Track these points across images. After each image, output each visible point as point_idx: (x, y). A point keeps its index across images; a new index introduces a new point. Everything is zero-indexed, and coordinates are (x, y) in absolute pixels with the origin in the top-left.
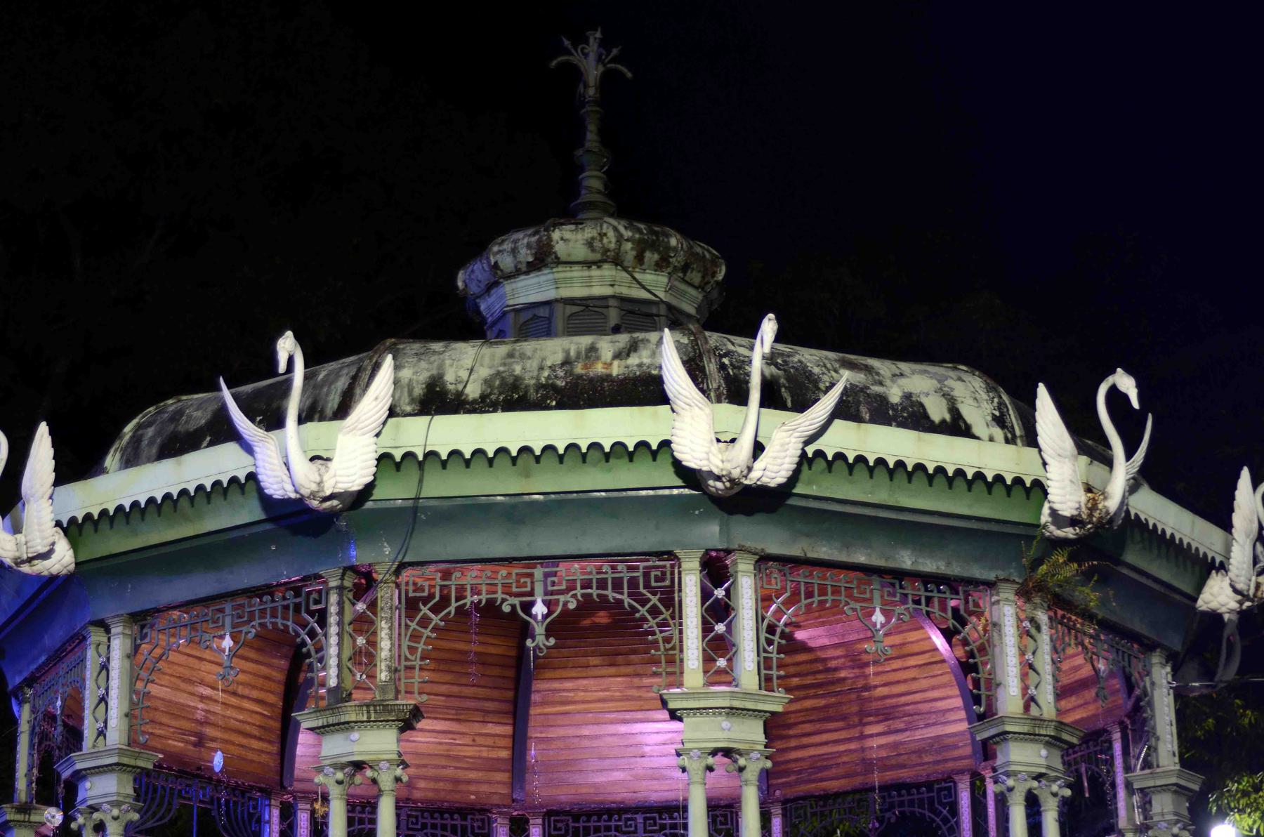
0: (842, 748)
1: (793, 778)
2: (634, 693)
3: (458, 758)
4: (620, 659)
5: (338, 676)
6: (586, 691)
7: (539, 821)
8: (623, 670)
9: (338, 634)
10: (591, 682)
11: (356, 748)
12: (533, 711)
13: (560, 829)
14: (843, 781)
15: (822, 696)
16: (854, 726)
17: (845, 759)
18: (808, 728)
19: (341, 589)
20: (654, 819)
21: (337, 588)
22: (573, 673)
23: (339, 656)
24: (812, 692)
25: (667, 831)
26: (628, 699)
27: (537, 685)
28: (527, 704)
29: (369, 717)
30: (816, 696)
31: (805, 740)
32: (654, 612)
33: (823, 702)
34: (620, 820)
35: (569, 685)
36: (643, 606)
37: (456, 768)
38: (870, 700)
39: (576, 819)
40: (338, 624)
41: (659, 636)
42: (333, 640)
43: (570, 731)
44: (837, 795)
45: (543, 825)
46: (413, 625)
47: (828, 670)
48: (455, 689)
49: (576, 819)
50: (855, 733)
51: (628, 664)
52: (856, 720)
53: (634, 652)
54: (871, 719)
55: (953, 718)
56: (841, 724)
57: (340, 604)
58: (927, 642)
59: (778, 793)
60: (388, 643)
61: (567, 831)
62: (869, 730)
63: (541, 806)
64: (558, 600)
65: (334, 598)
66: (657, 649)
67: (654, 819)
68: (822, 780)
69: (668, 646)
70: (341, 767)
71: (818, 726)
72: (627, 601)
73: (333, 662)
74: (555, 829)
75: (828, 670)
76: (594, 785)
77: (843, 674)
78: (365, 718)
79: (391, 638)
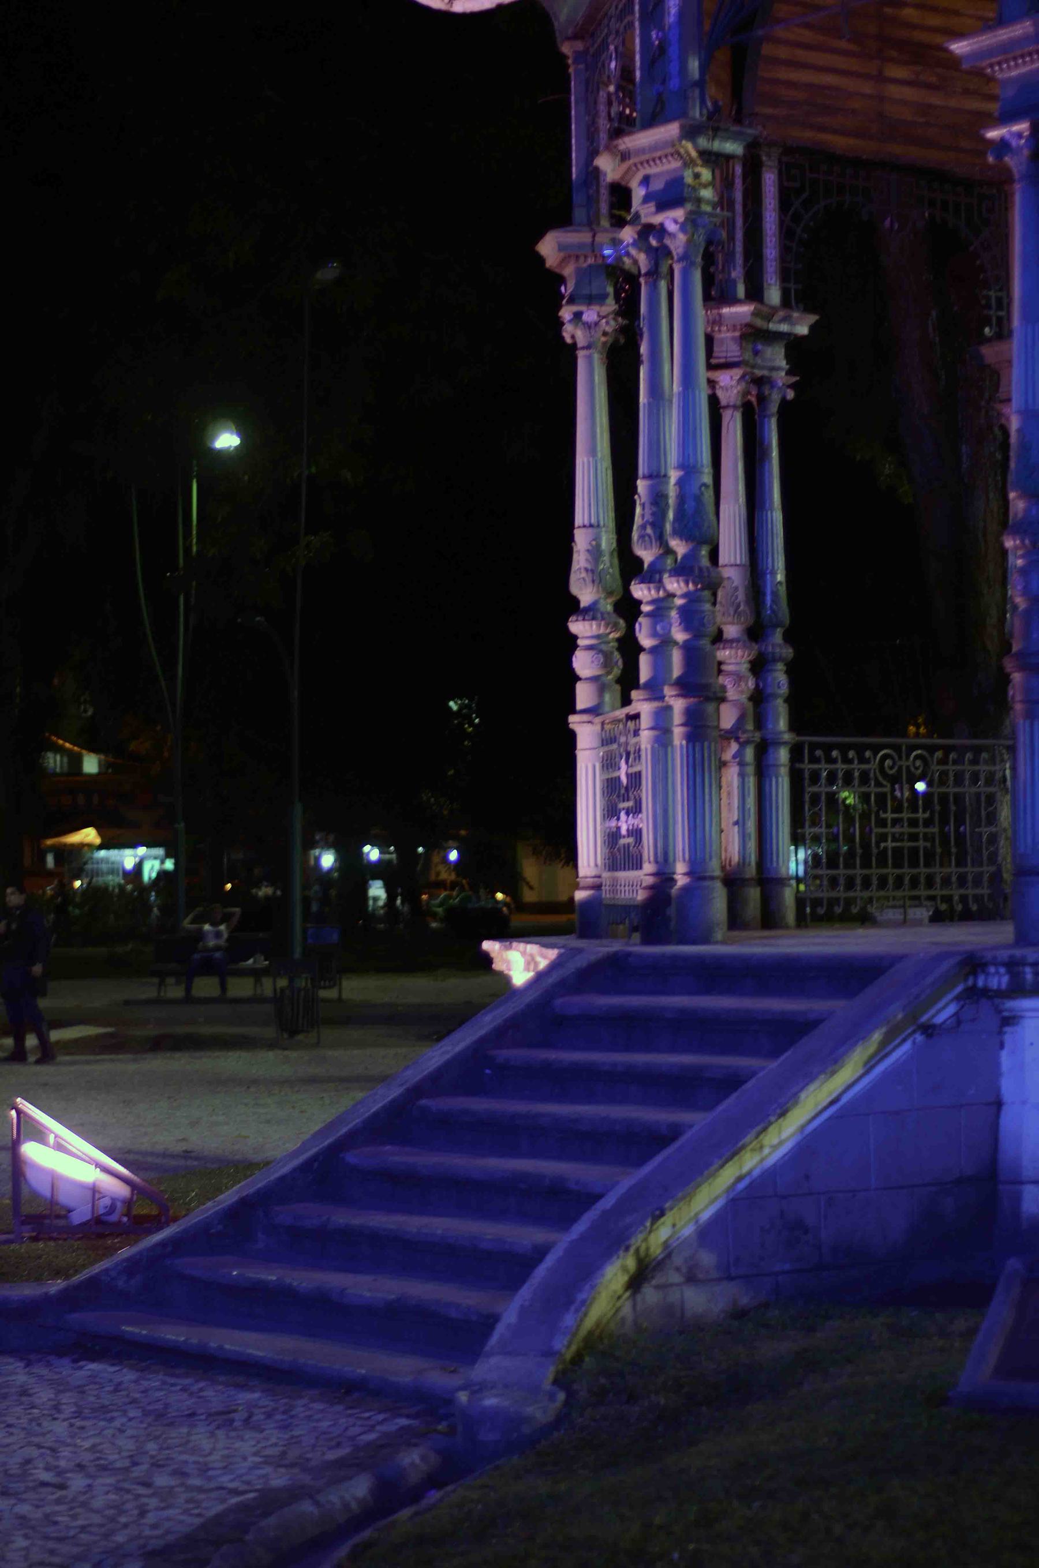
14: (852, 141)
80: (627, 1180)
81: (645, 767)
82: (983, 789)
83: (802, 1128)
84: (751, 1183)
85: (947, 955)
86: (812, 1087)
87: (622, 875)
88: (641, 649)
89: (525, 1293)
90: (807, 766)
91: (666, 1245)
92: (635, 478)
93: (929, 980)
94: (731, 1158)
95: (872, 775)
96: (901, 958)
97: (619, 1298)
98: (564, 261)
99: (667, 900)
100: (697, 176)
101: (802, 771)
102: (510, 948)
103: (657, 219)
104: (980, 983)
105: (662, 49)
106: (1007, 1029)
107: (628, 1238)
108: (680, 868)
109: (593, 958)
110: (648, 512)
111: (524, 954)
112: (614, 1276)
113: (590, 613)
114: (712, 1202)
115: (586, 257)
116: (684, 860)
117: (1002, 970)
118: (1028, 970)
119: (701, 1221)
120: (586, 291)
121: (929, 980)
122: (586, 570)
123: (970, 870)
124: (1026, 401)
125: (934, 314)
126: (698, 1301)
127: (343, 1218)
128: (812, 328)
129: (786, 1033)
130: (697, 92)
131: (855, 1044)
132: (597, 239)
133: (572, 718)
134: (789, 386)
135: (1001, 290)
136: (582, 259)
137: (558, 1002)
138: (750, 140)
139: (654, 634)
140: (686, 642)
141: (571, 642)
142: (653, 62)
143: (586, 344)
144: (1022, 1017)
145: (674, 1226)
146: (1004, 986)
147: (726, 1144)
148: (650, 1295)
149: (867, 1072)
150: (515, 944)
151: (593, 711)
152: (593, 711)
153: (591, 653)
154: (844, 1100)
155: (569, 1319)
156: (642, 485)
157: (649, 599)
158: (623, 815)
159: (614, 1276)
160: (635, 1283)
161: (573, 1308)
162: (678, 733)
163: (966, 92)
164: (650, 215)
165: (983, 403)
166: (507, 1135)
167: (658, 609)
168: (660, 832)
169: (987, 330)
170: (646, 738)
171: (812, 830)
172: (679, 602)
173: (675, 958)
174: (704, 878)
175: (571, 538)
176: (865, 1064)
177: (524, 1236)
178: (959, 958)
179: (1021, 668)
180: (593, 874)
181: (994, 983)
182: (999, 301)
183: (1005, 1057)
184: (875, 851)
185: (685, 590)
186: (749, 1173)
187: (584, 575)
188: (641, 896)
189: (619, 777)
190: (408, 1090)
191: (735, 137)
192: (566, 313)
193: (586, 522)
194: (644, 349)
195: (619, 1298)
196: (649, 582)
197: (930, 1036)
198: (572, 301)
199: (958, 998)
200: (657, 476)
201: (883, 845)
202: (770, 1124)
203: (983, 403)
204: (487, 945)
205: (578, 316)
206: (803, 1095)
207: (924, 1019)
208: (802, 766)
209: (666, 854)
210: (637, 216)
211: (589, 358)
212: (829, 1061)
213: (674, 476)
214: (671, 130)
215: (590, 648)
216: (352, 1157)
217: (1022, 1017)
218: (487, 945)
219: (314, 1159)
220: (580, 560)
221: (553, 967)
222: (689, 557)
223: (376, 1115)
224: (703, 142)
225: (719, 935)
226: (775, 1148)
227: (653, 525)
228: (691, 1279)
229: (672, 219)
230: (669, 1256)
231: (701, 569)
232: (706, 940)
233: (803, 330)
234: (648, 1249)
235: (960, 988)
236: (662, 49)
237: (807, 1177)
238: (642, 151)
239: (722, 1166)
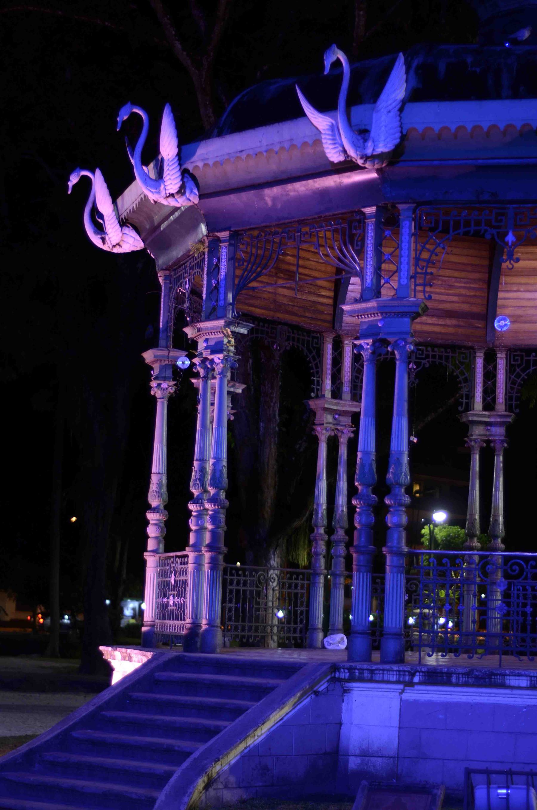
14: (263, 311)
32: (314, 358)
36: (521, 375)
38: (283, 261)
46: (513, 377)
55: (323, 293)
58: (512, 320)
64: (421, 362)
72: (305, 350)
74: (514, 360)
80: (202, 747)
81: (190, 579)
82: (299, 591)
83: (269, 730)
84: (249, 751)
85: (323, 664)
86: (274, 713)
87: (168, 622)
88: (191, 530)
89: (167, 788)
90: (228, 577)
91: (218, 773)
92: (193, 460)
93: (318, 673)
94: (243, 741)
95: (255, 582)
96: (305, 664)
97: (201, 792)
98: (154, 362)
99: (197, 634)
100: (229, 342)
101: (227, 579)
102: (116, 650)
103: (211, 357)
104: (337, 676)
105: (217, 288)
106: (345, 694)
107: (206, 769)
108: (204, 622)
109: (170, 657)
110: (198, 474)
111: (121, 653)
112: (201, 783)
113: (155, 510)
114: (235, 757)
115: (165, 361)
116: (206, 618)
117: (346, 671)
118: (357, 671)
119: (231, 764)
120: (163, 375)
121: (318, 673)
122: (156, 492)
123: (247, 624)
124: (364, 448)
125: (251, 361)
126: (228, 796)
127: (75, 758)
128: (243, 390)
129: (258, 693)
130: (231, 307)
131: (290, 697)
132: (170, 354)
133: (145, 554)
134: (232, 414)
135: (319, 377)
136: (163, 362)
137: (157, 674)
138: (250, 328)
139: (197, 525)
140: (212, 529)
141: (147, 523)
142: (211, 292)
143: (162, 397)
144: (352, 690)
145: (221, 765)
146: (346, 677)
147: (242, 734)
148: (212, 792)
149: (294, 709)
150: (118, 649)
151: (155, 551)
152: (155, 551)
153: (156, 527)
154: (285, 719)
155: (186, 799)
156: (195, 463)
157: (196, 510)
158: (171, 597)
159: (201, 783)
160: (207, 787)
161: (187, 795)
162: (206, 568)
163: (310, 293)
164: (206, 354)
165: (272, 404)
166: (140, 727)
167: (199, 514)
168: (195, 606)
169: (312, 394)
170: (190, 567)
171: (229, 605)
172: (210, 513)
173: (206, 659)
174: (214, 626)
175: (150, 478)
176: (293, 705)
177: (161, 768)
178: (329, 666)
179: (357, 552)
180: (151, 620)
181: (342, 676)
182: (318, 381)
183: (344, 706)
184: (254, 615)
185: (214, 508)
186: (250, 745)
187: (155, 494)
188: (185, 632)
189: (169, 581)
190: (97, 707)
191: (245, 327)
192: (154, 384)
193: (157, 472)
194: (200, 407)
195: (201, 792)
196: (197, 503)
197: (317, 696)
198: (156, 378)
199: (328, 681)
200: (202, 460)
201: (257, 613)
202: (259, 726)
203: (272, 404)
204: (101, 648)
205: (159, 385)
206: (271, 716)
207: (315, 689)
208: (227, 577)
209: (196, 616)
210: (201, 354)
211: (163, 403)
212: (281, 704)
213: (212, 461)
214: (221, 322)
215: (155, 525)
216: (75, 734)
217: (352, 690)
218: (101, 648)
219: (58, 735)
220: (153, 487)
221: (149, 662)
222: (216, 495)
223: (84, 717)
224: (233, 328)
225: (218, 650)
226: (259, 736)
227: (200, 480)
228: (226, 787)
229: (218, 358)
230: (219, 777)
231: (220, 500)
232: (213, 652)
233: (239, 391)
234: (212, 774)
235: (329, 677)
236: (217, 288)
237: (270, 749)
238: (207, 329)
239: (241, 743)
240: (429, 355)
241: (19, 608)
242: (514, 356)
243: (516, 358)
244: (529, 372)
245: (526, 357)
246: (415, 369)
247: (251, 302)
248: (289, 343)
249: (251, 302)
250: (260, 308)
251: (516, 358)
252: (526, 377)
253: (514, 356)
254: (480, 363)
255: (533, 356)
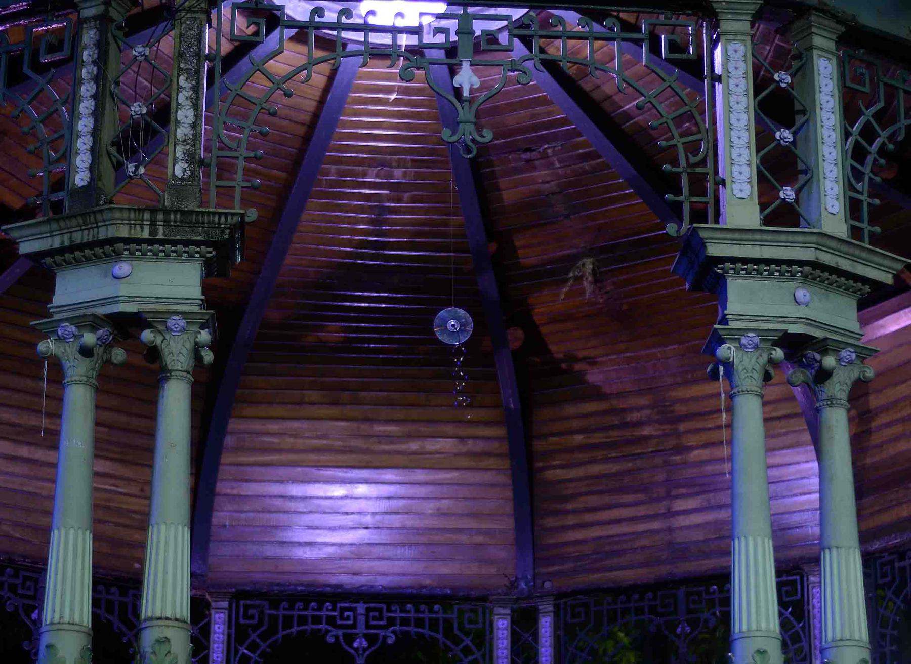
0: (641, 527)
1: (569, 565)
2: (359, 443)
3: (120, 511)
4: (345, 395)
5: (91, 168)
6: (295, 436)
7: (225, 604)
8: (348, 410)
9: (95, 97)
10: (305, 425)
11: (123, 289)
12: (226, 458)
13: (252, 617)
14: (640, 571)
15: (615, 460)
16: (659, 500)
17: (644, 542)
18: (593, 500)
19: (103, 20)
20: (380, 610)
21: (95, 18)
22: (279, 411)
23: (95, 133)
24: (599, 454)
25: (397, 628)
26: (351, 451)
27: (233, 424)
28: (219, 450)
29: (153, 233)
30: (606, 460)
31: (588, 517)
33: (614, 468)
34: (334, 610)
35: (273, 427)
37: (117, 524)
38: (685, 464)
39: (275, 605)
40: (96, 79)
41: (679, 141)
42: (86, 107)
43: (275, 489)
44: (634, 588)
45: (230, 610)
47: (625, 425)
48: (123, 419)
49: (275, 605)
50: (661, 508)
51: (356, 402)
52: (662, 491)
53: (365, 388)
54: (683, 491)
56: (640, 496)
57: (102, 46)
59: (548, 584)
60: (191, 113)
61: (261, 620)
62: (680, 505)
63: (230, 585)
65: (89, 36)
66: (675, 162)
67: (380, 610)
68: (611, 569)
69: (693, 160)
70: (94, 322)
71: (606, 499)
73: (83, 144)
74: (246, 616)
75: (625, 425)
76: (301, 561)
77: (646, 431)
78: (146, 235)
79: (196, 106)
240: (394, 619)
241: (54, 214)
242: (247, 607)
243: (251, 612)
244: (276, 641)
245: (270, 609)
246: (365, 650)
247: (608, 563)
248: (714, 614)
249: (608, 563)
250: (631, 567)
251: (346, 614)
252: (269, 650)
253: (247, 607)
254: (502, 626)
255: (285, 609)
